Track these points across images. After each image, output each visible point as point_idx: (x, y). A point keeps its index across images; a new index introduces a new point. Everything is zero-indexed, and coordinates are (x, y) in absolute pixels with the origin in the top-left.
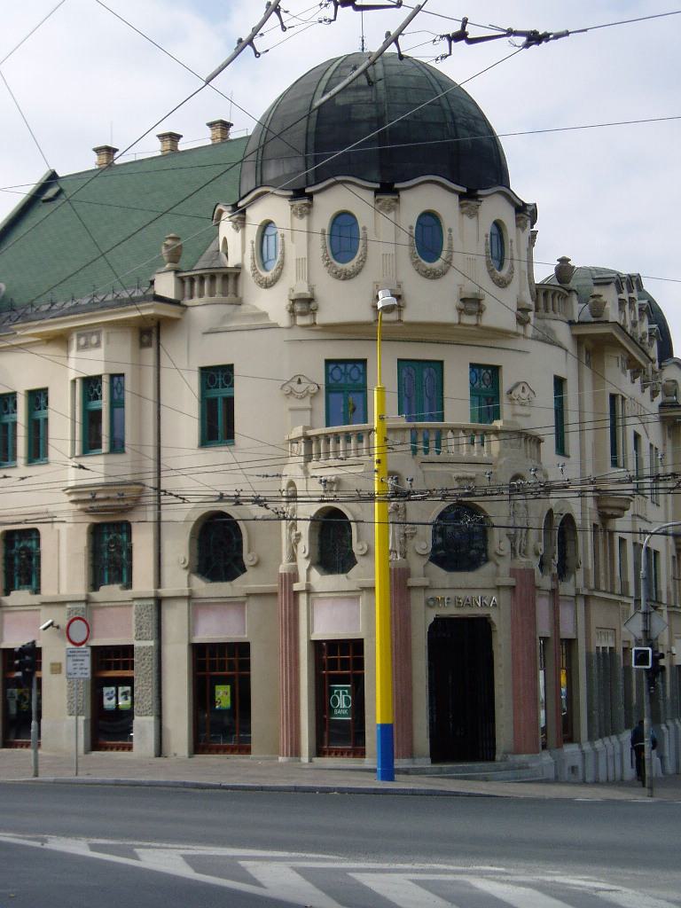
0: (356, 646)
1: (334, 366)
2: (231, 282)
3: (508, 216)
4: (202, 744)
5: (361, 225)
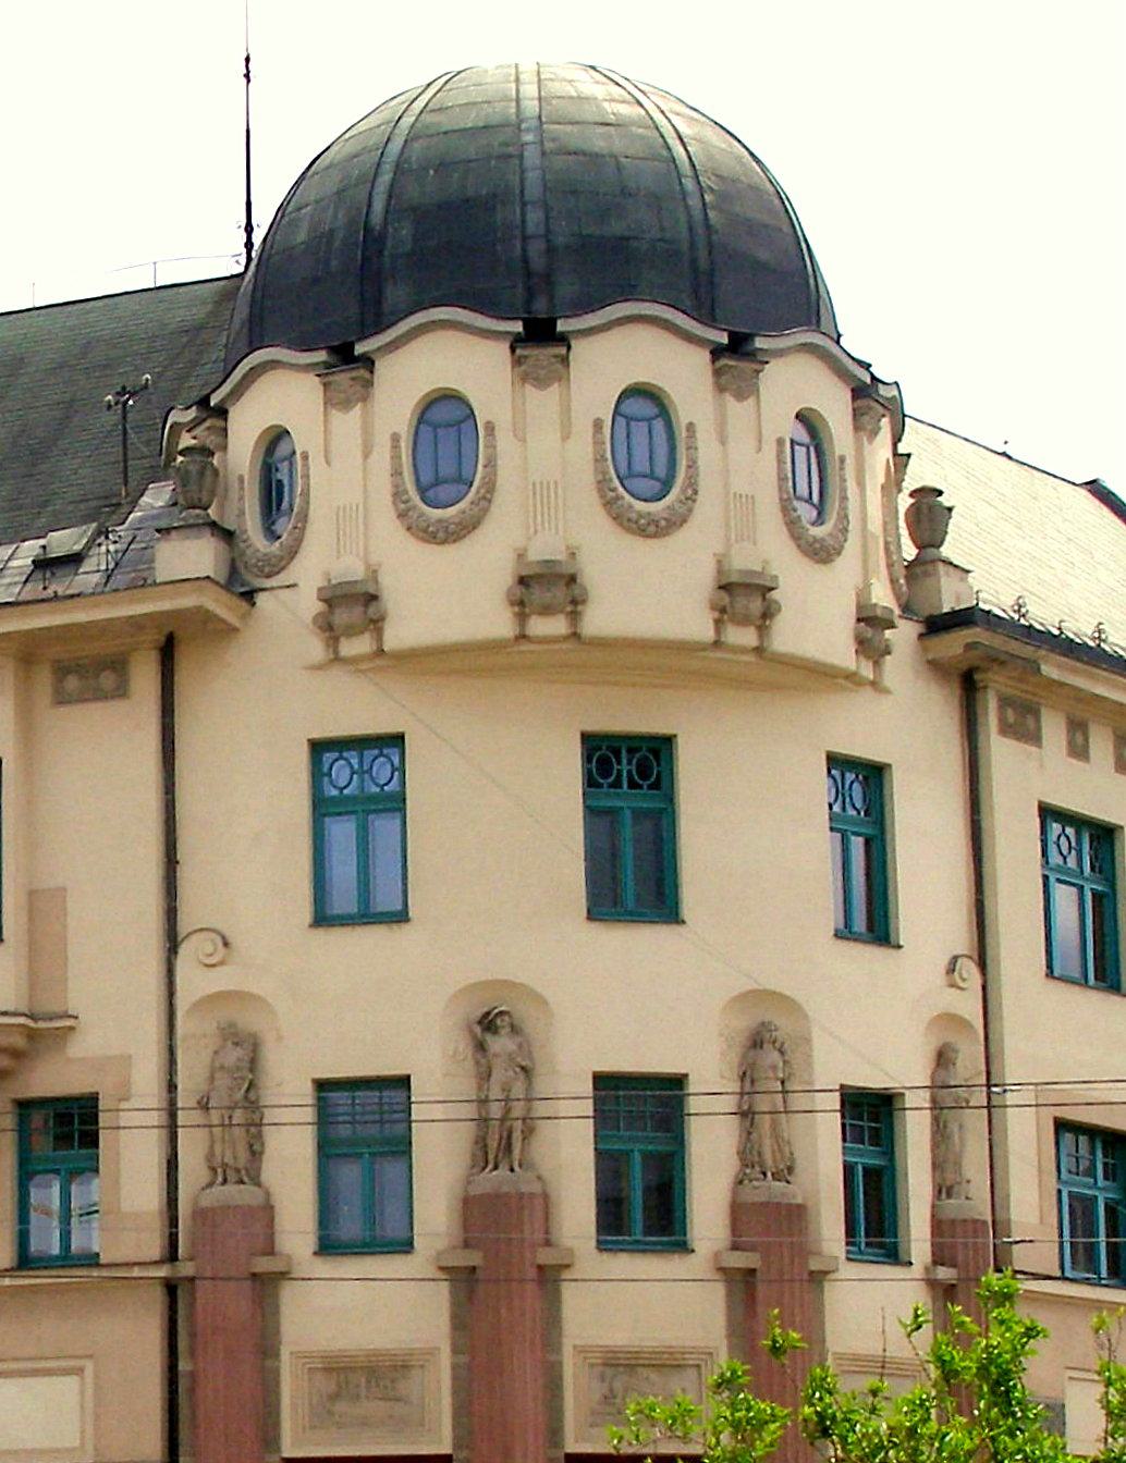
3: (835, 407)
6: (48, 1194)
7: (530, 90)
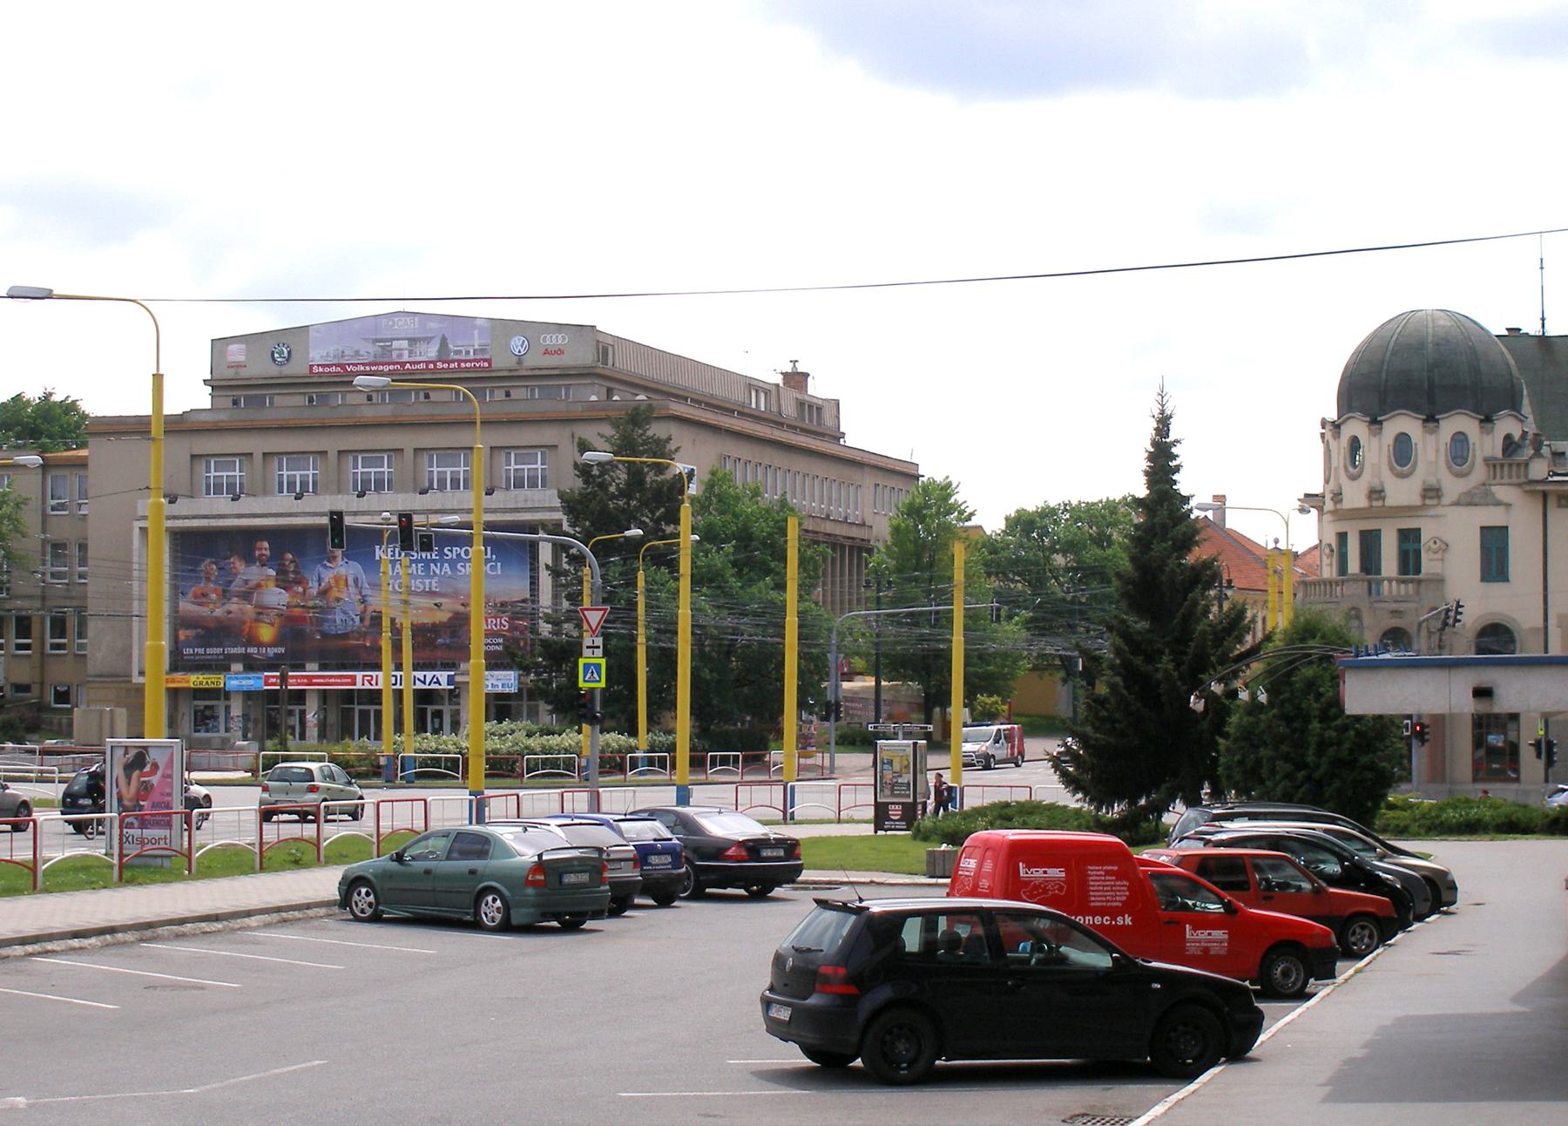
2: (1522, 468)
7: (1430, 324)
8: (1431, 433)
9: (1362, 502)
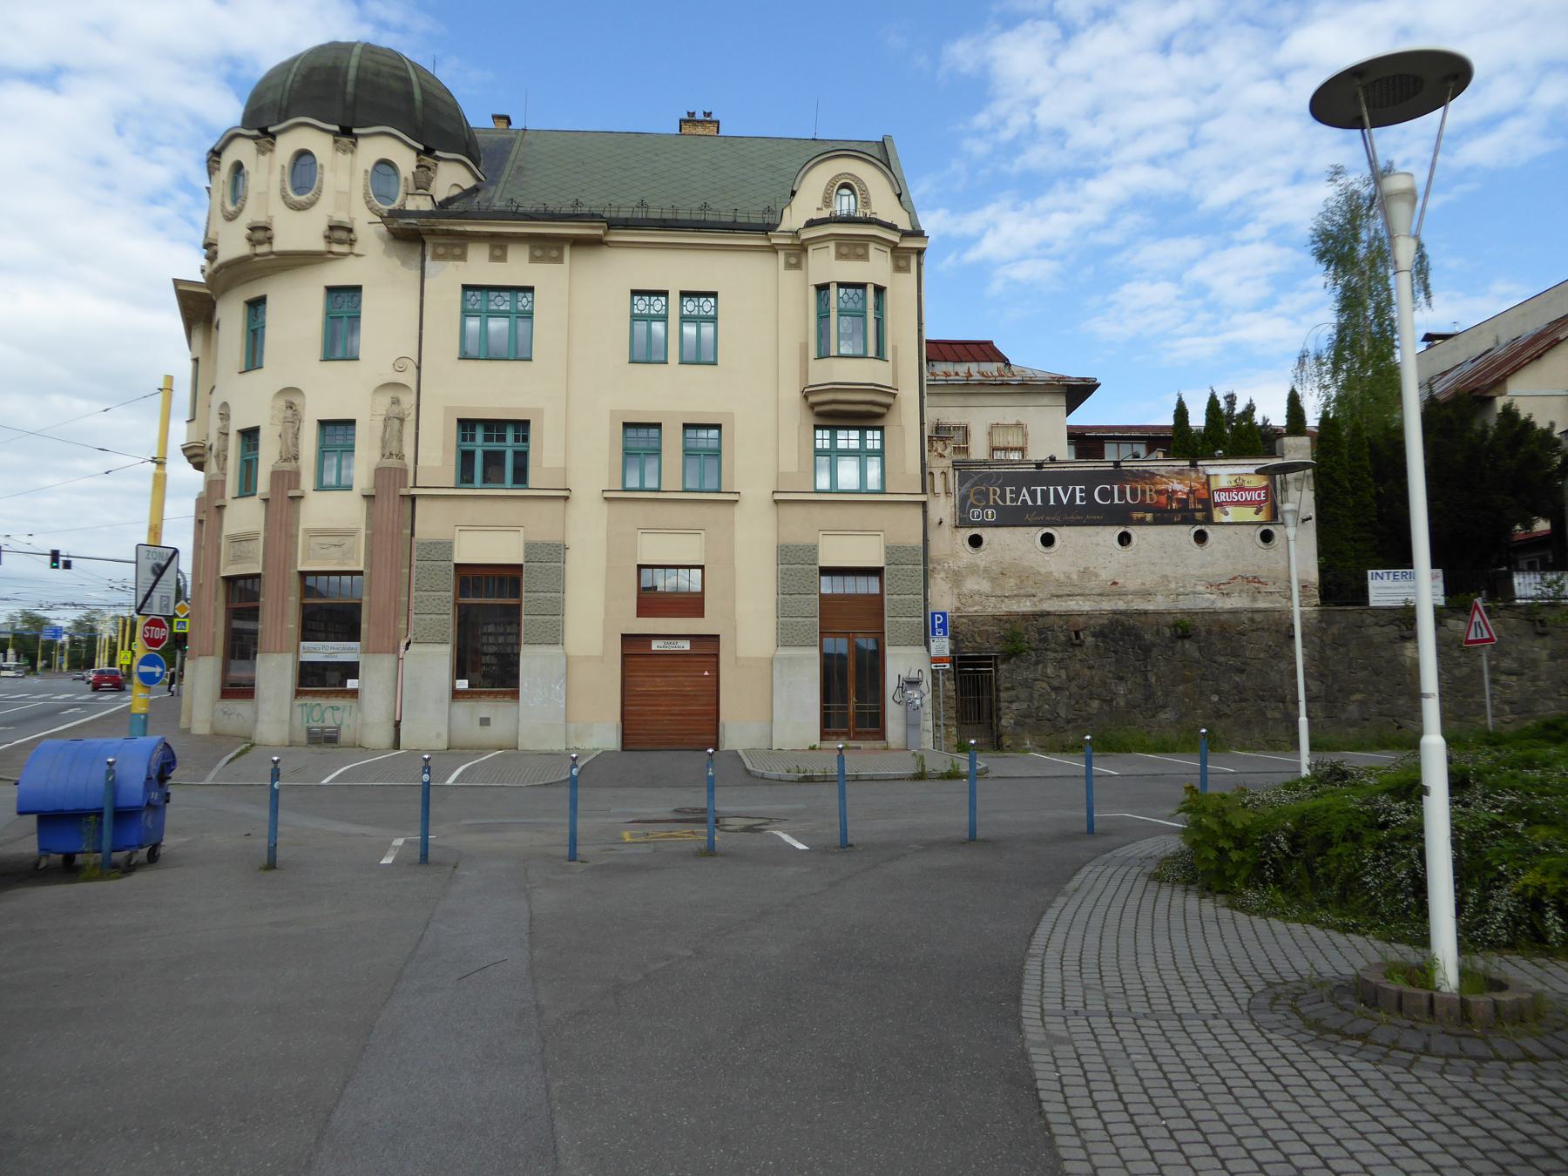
0: (700, 613)
1: (497, 294)
4: (1353, 858)
5: (319, 162)
6: (332, 462)
8: (344, 151)
9: (243, 249)
